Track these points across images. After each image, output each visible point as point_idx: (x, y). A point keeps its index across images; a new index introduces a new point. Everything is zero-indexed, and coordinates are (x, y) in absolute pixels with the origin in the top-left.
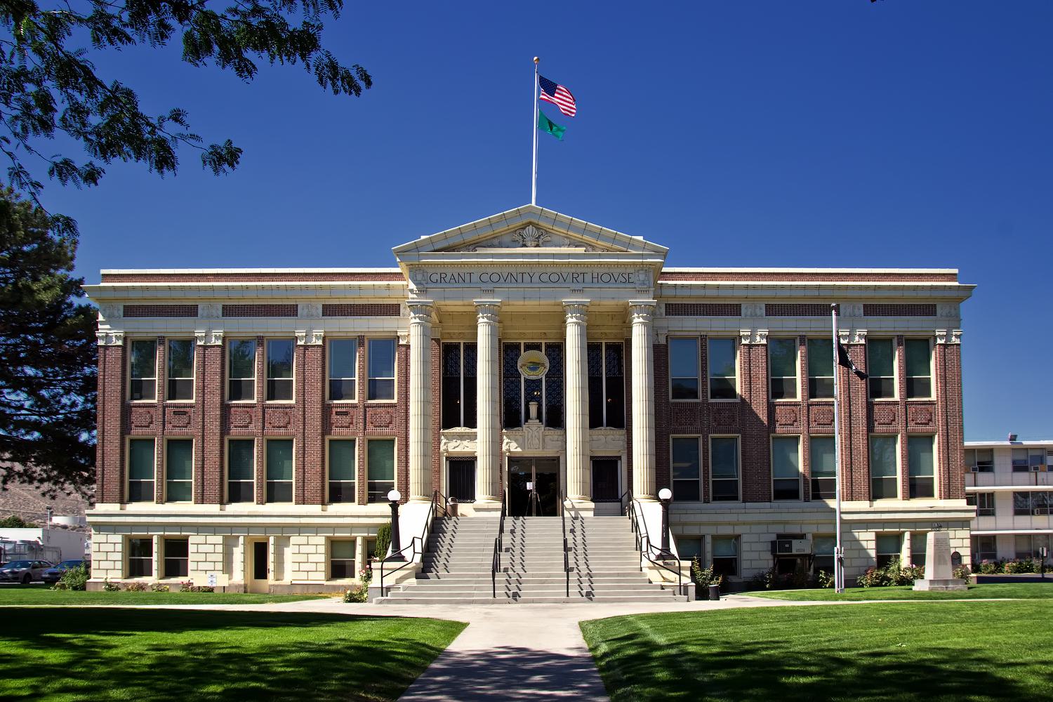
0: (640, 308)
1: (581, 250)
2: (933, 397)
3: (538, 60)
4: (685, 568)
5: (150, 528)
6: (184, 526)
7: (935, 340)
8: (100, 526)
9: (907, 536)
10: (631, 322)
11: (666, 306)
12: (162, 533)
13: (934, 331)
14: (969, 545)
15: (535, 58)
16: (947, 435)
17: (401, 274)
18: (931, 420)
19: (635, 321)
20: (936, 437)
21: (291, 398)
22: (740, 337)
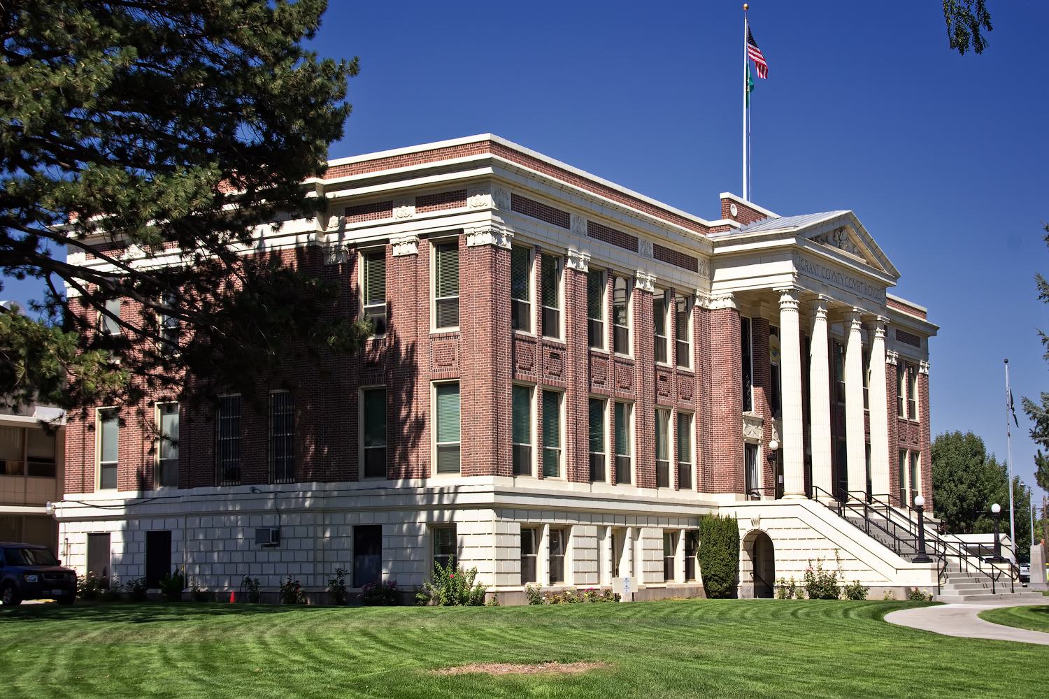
0: (823, 303)
1: (863, 261)
2: (562, 339)
3: (747, 8)
4: (315, 580)
5: (569, 515)
6: (650, 516)
7: (566, 261)
8: (502, 509)
9: (546, 531)
10: (814, 316)
11: (464, 191)
12: (601, 524)
13: (567, 250)
14: (520, 545)
15: (746, 5)
16: (703, 417)
17: (925, 313)
18: (561, 371)
19: (877, 335)
20: (565, 395)
21: (440, 325)
22: (566, 258)
